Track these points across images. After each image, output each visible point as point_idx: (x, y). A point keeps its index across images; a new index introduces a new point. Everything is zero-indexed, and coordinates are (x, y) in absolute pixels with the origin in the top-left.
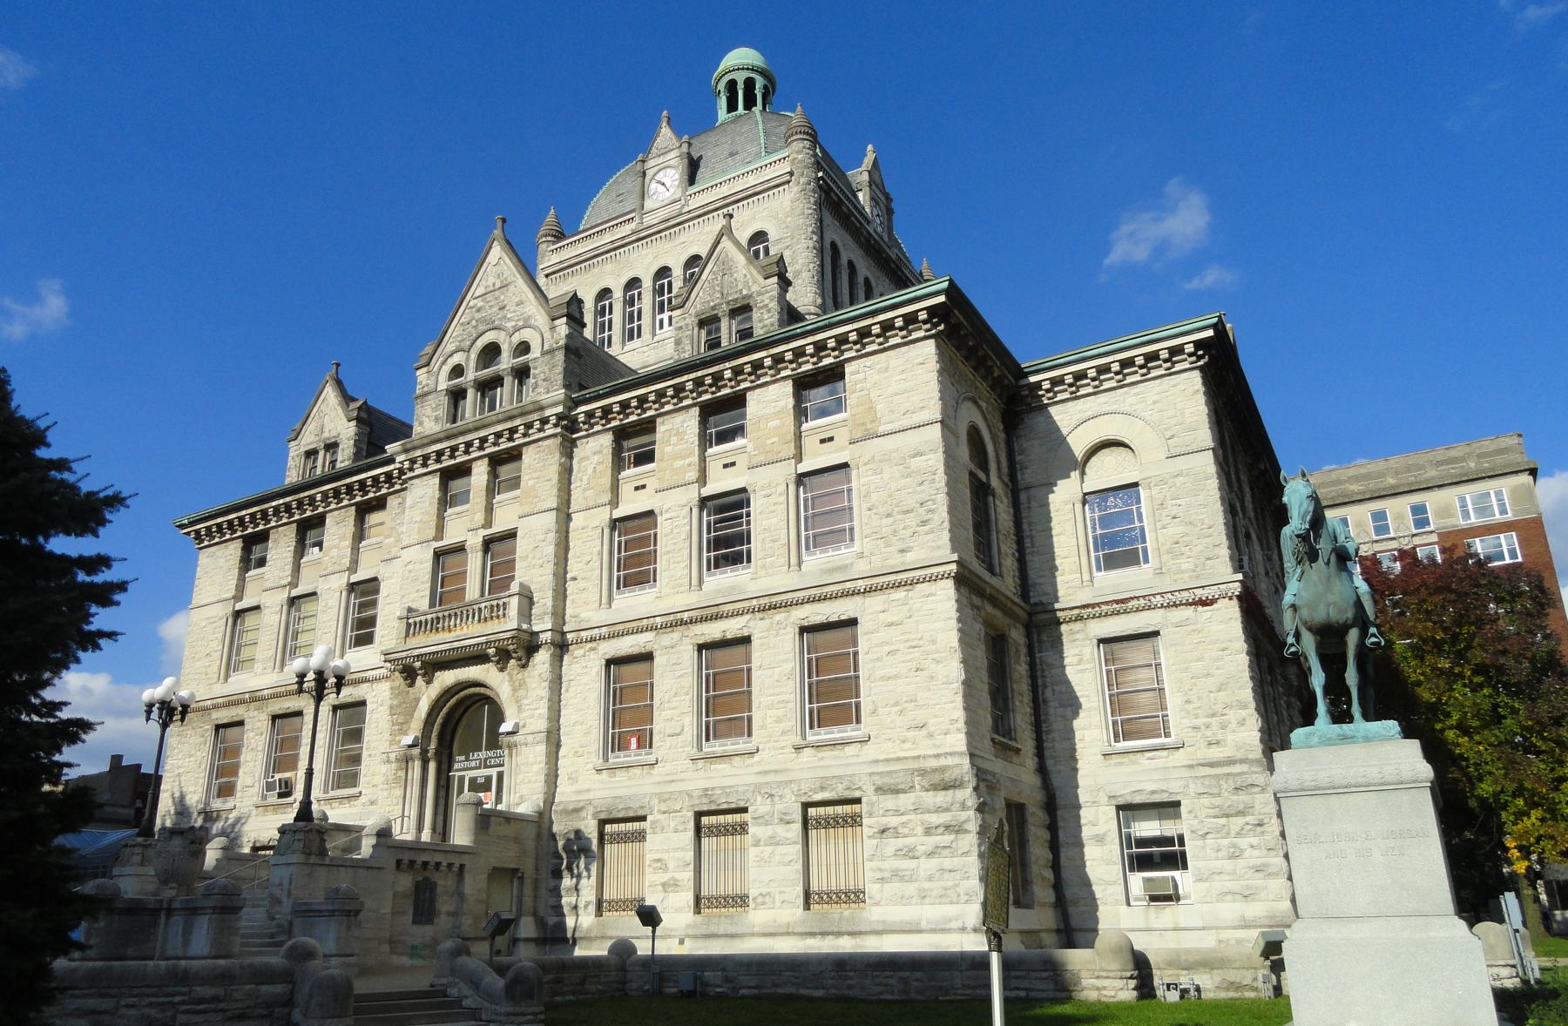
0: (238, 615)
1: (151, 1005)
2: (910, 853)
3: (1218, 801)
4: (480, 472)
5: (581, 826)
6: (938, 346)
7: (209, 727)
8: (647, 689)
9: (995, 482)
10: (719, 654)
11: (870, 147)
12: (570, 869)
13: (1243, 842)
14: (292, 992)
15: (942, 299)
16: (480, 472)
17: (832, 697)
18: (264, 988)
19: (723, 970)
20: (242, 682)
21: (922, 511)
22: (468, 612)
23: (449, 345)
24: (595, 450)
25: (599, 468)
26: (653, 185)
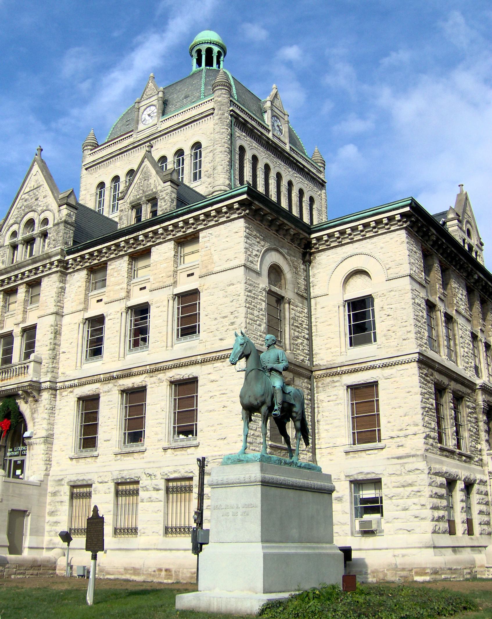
4: (22, 290)
11: (274, 86)
20: (97, 367)
21: (232, 317)
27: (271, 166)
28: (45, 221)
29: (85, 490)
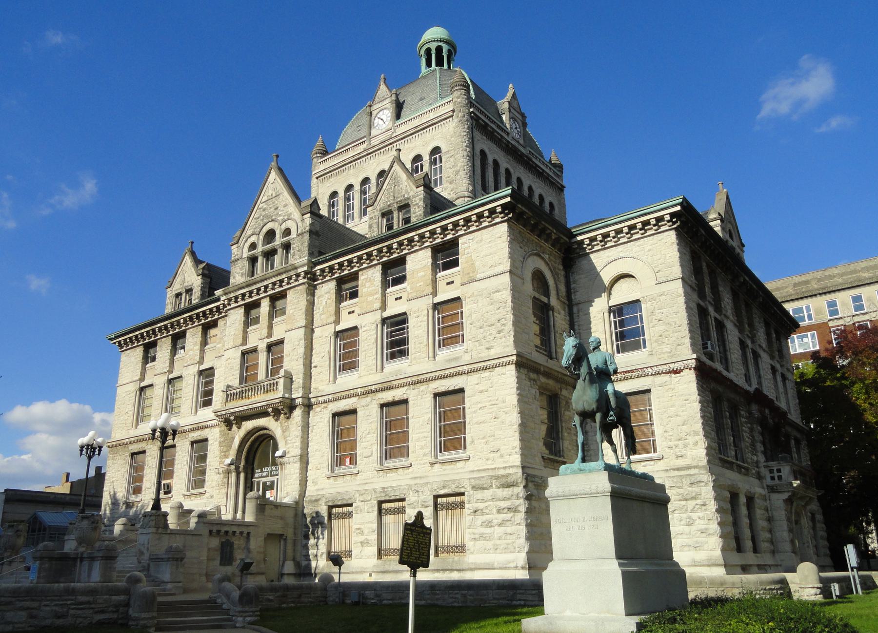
0: (142, 389)
1: (56, 605)
2: (489, 524)
3: (680, 491)
4: (265, 305)
5: (319, 509)
6: (509, 227)
7: (128, 454)
8: (353, 430)
9: (554, 302)
10: (393, 409)
11: (511, 86)
12: (313, 534)
13: (695, 516)
14: (129, 600)
15: (508, 199)
16: (265, 305)
17: (451, 434)
18: (114, 597)
19: (375, 590)
21: (499, 324)
22: (258, 388)
23: (249, 231)
24: (327, 290)
25: (329, 301)
26: (377, 120)
27: (512, 171)
28: (287, 232)
29: (344, 509)
